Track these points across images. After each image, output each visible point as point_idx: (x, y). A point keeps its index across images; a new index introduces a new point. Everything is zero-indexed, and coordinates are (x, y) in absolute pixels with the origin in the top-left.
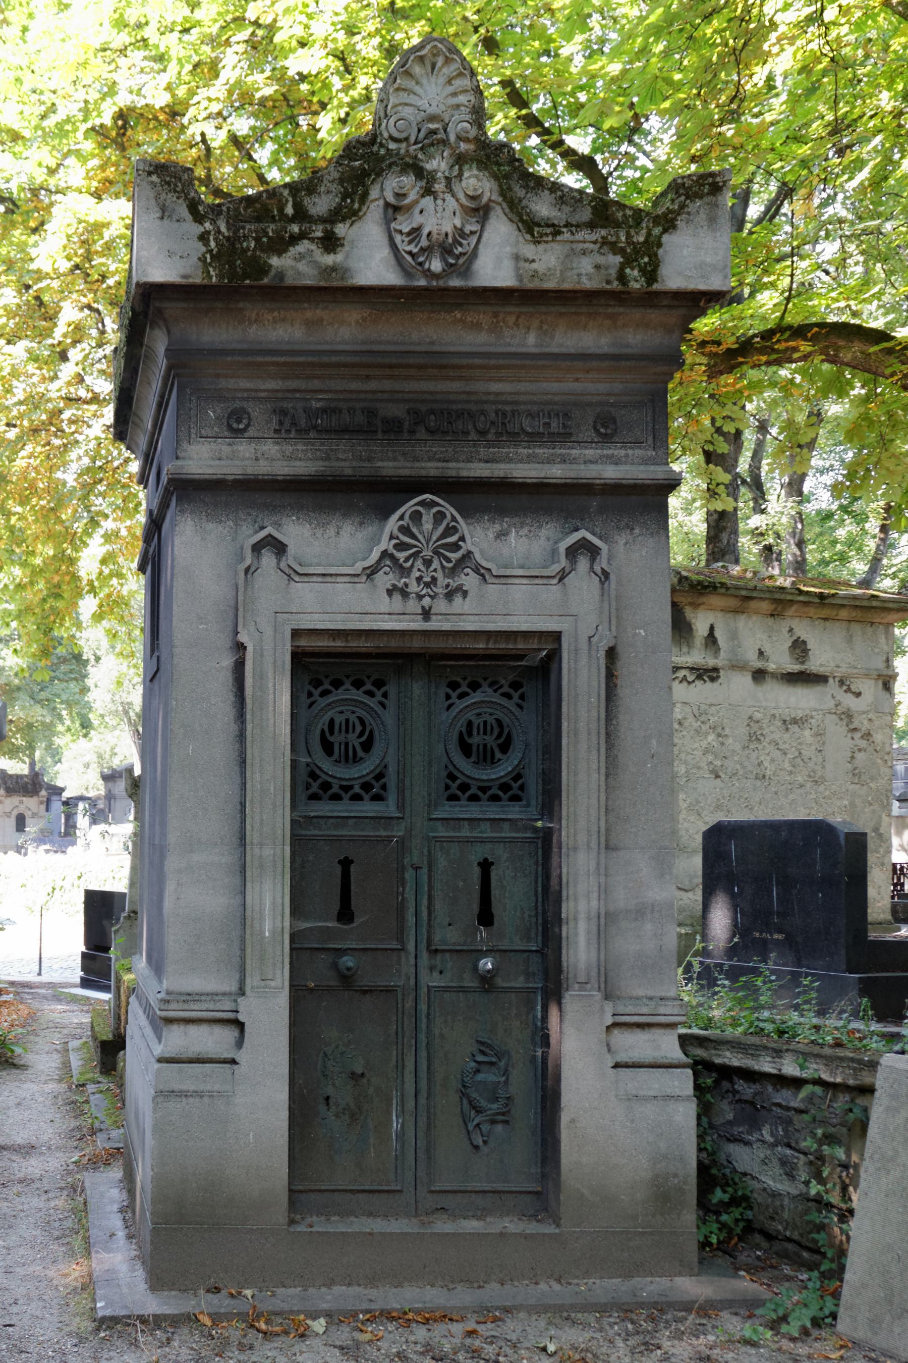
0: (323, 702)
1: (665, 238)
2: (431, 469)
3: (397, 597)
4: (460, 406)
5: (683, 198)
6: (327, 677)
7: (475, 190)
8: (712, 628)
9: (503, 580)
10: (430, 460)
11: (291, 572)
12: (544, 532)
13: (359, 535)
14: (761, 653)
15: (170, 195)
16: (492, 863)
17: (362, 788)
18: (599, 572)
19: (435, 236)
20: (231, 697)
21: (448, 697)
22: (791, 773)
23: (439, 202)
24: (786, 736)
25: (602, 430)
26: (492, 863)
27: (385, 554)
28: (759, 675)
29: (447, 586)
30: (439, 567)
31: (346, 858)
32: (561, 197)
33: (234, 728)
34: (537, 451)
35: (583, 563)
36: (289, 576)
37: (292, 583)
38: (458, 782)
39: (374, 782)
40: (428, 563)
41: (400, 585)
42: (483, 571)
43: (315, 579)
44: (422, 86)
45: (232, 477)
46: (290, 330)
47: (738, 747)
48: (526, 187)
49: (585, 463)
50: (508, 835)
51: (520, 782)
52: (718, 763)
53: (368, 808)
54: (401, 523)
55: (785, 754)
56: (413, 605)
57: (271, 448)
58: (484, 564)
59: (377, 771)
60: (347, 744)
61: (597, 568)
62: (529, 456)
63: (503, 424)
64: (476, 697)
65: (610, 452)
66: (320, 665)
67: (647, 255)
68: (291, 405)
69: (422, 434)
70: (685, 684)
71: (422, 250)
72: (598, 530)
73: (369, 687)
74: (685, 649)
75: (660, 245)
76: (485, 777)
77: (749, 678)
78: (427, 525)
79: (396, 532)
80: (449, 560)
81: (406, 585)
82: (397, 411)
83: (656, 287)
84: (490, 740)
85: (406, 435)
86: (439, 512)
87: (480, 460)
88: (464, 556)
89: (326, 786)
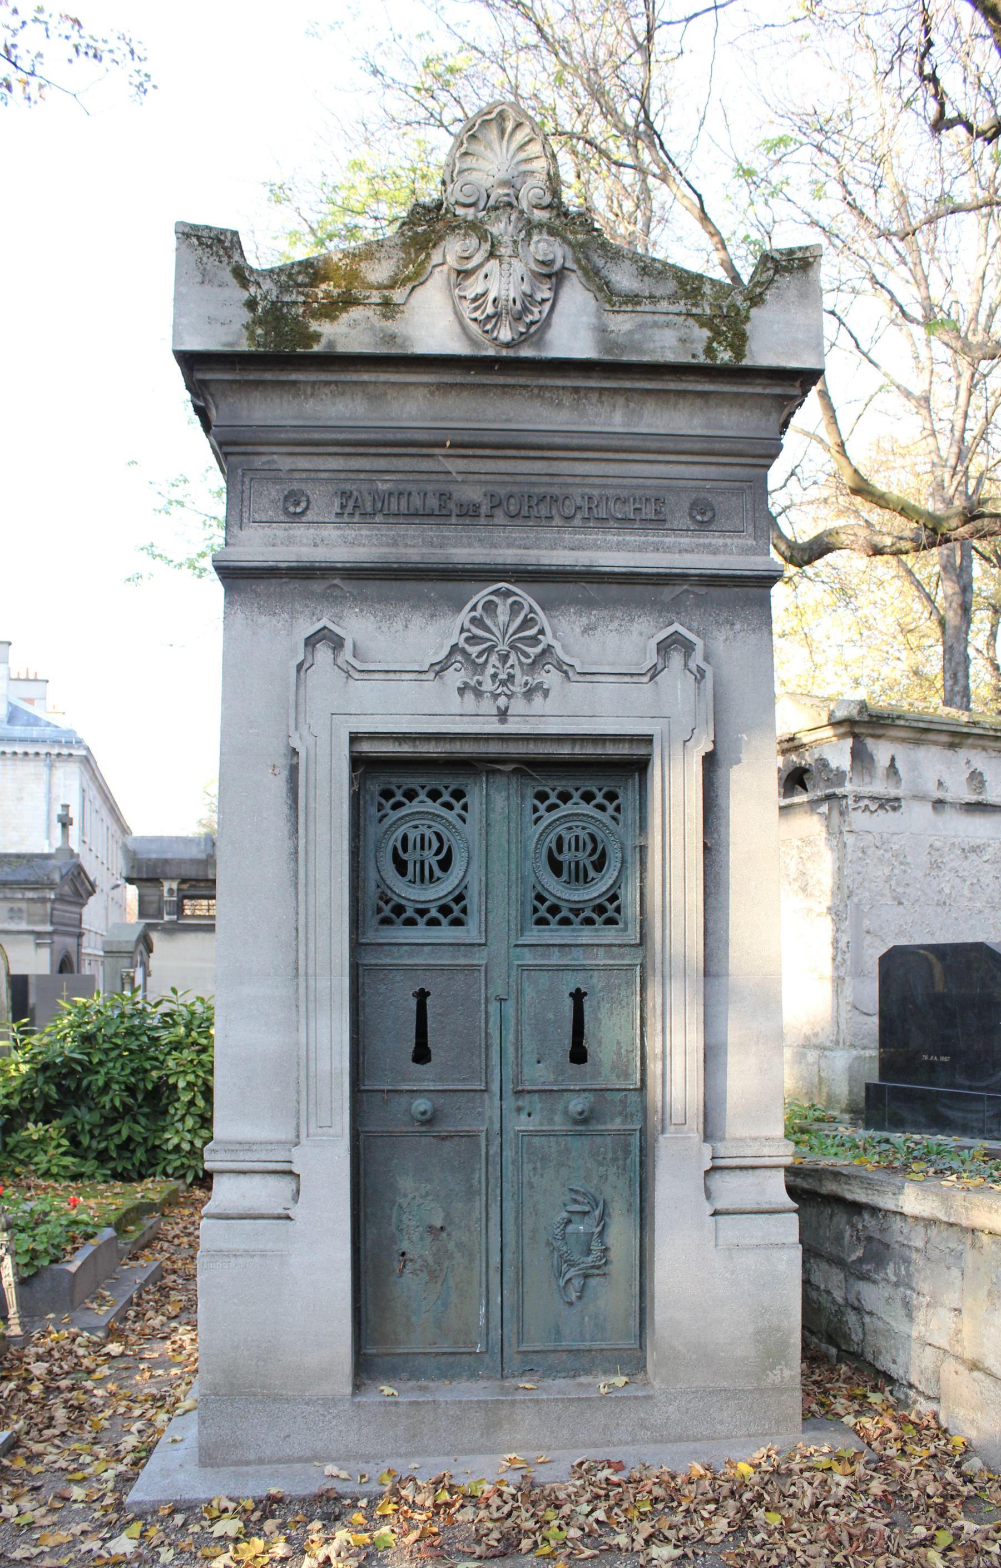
0: (395, 815)
1: (754, 312)
2: (508, 556)
3: (469, 696)
4: (543, 490)
5: (771, 272)
6: (399, 787)
7: (545, 255)
8: (893, 759)
9: (589, 678)
10: (509, 546)
11: (350, 668)
12: (636, 627)
13: (431, 629)
14: (940, 784)
15: (212, 259)
16: (585, 994)
17: (439, 911)
18: (694, 670)
19: (501, 304)
20: (285, 810)
21: (536, 809)
22: (970, 899)
23: (505, 266)
24: (965, 864)
25: (699, 518)
26: (585, 994)
27: (454, 648)
28: (939, 804)
29: (526, 684)
30: (517, 663)
31: (422, 990)
32: (644, 269)
33: (287, 845)
34: (627, 538)
35: (676, 659)
36: (347, 672)
37: (351, 681)
38: (547, 904)
39: (453, 905)
40: (504, 658)
41: (473, 683)
42: (565, 668)
43: (376, 676)
44: (492, 150)
45: (286, 565)
46: (351, 406)
47: (920, 875)
48: (605, 256)
49: (680, 552)
50: (602, 963)
51: (615, 904)
52: (901, 890)
53: (446, 933)
54: (473, 614)
55: (965, 881)
56: (488, 706)
57: (331, 532)
58: (567, 660)
59: (457, 893)
60: (422, 863)
61: (692, 666)
62: (618, 543)
63: (590, 508)
64: (566, 809)
65: (707, 541)
66: (385, 773)
67: (730, 323)
68: (354, 487)
69: (500, 518)
70: (868, 813)
71: (489, 318)
72: (695, 625)
73: (446, 797)
74: (867, 779)
75: (747, 318)
76: (576, 898)
77: (929, 807)
78: (503, 613)
79: (467, 625)
80: (527, 656)
81: (480, 683)
82: (473, 494)
83: (746, 362)
84: (583, 857)
85: (483, 520)
86: (515, 603)
87: (565, 548)
88: (544, 652)
89: (399, 910)
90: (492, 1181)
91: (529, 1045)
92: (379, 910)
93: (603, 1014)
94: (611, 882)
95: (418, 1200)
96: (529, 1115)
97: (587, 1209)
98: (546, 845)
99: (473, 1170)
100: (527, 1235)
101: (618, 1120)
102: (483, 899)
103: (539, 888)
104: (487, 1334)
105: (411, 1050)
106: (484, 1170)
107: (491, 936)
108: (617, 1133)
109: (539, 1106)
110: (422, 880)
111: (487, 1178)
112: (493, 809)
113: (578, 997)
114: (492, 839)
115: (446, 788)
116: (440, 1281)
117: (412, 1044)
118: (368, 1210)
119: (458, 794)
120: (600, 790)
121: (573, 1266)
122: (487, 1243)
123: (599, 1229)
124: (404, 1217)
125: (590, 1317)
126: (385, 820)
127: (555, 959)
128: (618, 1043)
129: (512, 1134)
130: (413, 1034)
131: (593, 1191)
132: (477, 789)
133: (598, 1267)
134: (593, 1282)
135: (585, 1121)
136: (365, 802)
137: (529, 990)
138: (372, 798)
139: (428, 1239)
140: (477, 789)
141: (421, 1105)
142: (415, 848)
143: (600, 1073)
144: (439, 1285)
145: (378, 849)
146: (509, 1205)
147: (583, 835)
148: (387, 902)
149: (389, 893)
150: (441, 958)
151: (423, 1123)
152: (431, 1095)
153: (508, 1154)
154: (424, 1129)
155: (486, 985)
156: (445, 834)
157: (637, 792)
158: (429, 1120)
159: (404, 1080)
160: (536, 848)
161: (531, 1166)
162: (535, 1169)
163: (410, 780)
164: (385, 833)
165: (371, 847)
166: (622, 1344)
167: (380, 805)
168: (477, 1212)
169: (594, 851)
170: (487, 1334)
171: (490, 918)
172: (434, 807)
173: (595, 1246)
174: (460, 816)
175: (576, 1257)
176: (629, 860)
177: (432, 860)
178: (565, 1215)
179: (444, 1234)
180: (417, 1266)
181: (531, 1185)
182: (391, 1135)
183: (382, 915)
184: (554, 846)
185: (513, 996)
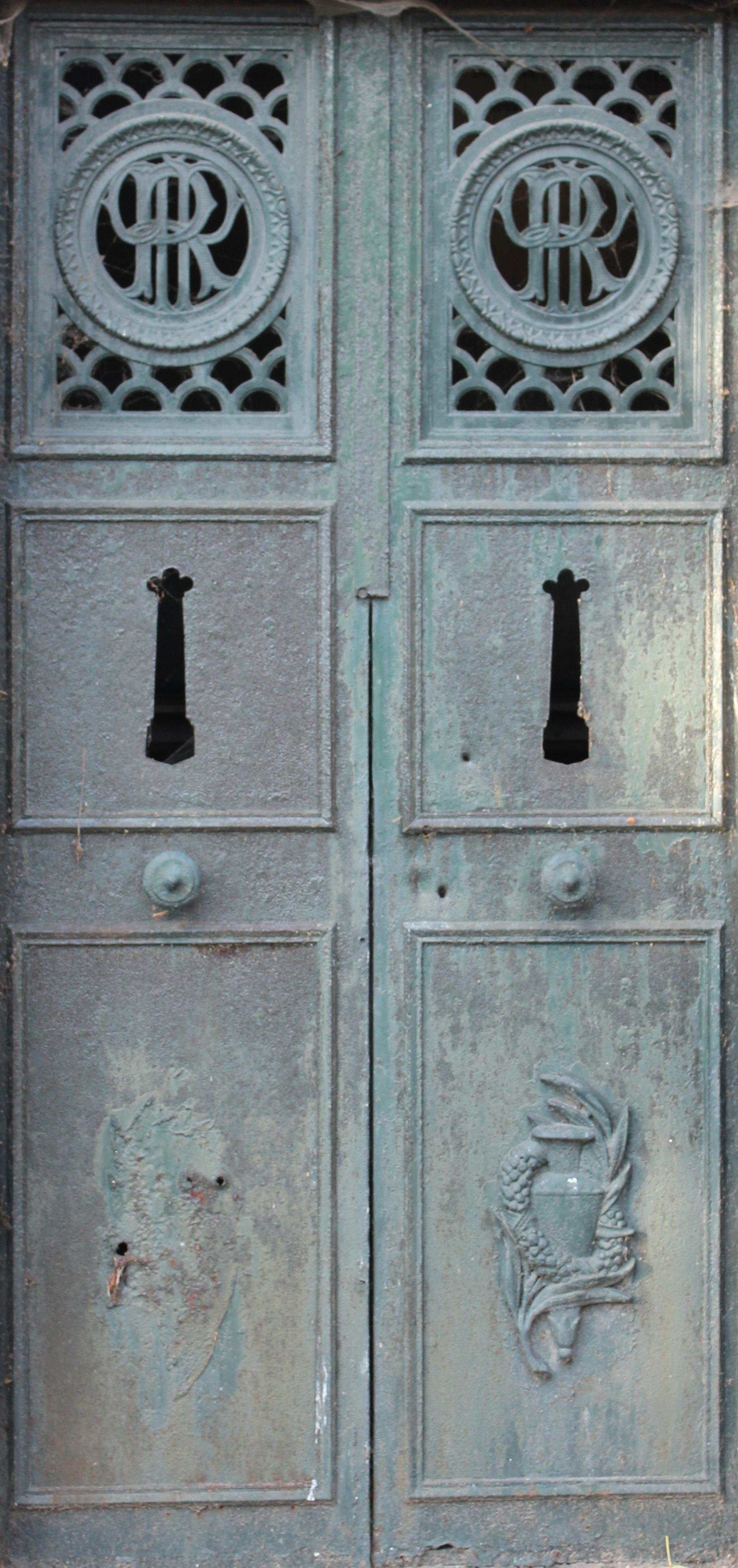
0: (104, 129)
16: (584, 585)
21: (460, 116)
26: (584, 585)
31: (172, 574)
38: (489, 356)
51: (661, 357)
53: (232, 429)
59: (259, 327)
64: (536, 115)
76: (562, 343)
84: (581, 238)
89: (113, 370)
90: (347, 1061)
91: (442, 715)
92: (64, 372)
93: (628, 636)
94: (650, 301)
95: (161, 1111)
96: (442, 892)
97: (586, 1132)
98: (485, 206)
99: (299, 1034)
100: (435, 1197)
101: (667, 906)
102: (327, 342)
103: (468, 317)
104: (335, 1456)
105: (143, 728)
106: (326, 1031)
107: (345, 436)
108: (664, 940)
109: (465, 869)
110: (172, 297)
111: (335, 1055)
112: (353, 117)
113: (566, 592)
114: (350, 190)
115: (234, 60)
116: (215, 1316)
117: (147, 710)
118: (34, 1136)
119: (264, 77)
120: (624, 66)
121: (550, 1278)
122: (334, 1219)
123: (618, 1184)
124: (126, 1154)
125: (595, 1410)
126: (78, 141)
127: (509, 495)
128: (667, 710)
129: (398, 941)
130: (149, 686)
131: (601, 1086)
132: (311, 63)
133: (616, 1283)
134: (602, 1321)
135: (582, 909)
136: (27, 97)
137: (442, 575)
138: (45, 86)
139: (186, 1208)
140: (311, 63)
141: (169, 865)
142: (153, 213)
143: (620, 787)
144: (211, 1330)
145: (59, 215)
146: (389, 1121)
147: (581, 182)
148: (83, 351)
149: (89, 328)
150: (218, 492)
151: (173, 913)
152: (195, 841)
153: (389, 991)
154: (174, 927)
155: (334, 561)
156: (231, 178)
157: (718, 71)
158: (188, 905)
159: (125, 803)
160: (461, 215)
161: (445, 1023)
162: (456, 1029)
163: (142, 40)
164: (79, 175)
165: (43, 209)
166: (678, 1482)
167: (65, 103)
168: (311, 1140)
169: (607, 221)
170: (335, 1456)
171: (344, 392)
172: (203, 109)
173: (608, 1227)
174: (268, 132)
175: (559, 1255)
176: (697, 244)
177: (197, 244)
178: (532, 1148)
179: (226, 1197)
180: (157, 1278)
181: (445, 1071)
182: (92, 943)
183: (70, 384)
184: (506, 210)
185: (402, 590)
